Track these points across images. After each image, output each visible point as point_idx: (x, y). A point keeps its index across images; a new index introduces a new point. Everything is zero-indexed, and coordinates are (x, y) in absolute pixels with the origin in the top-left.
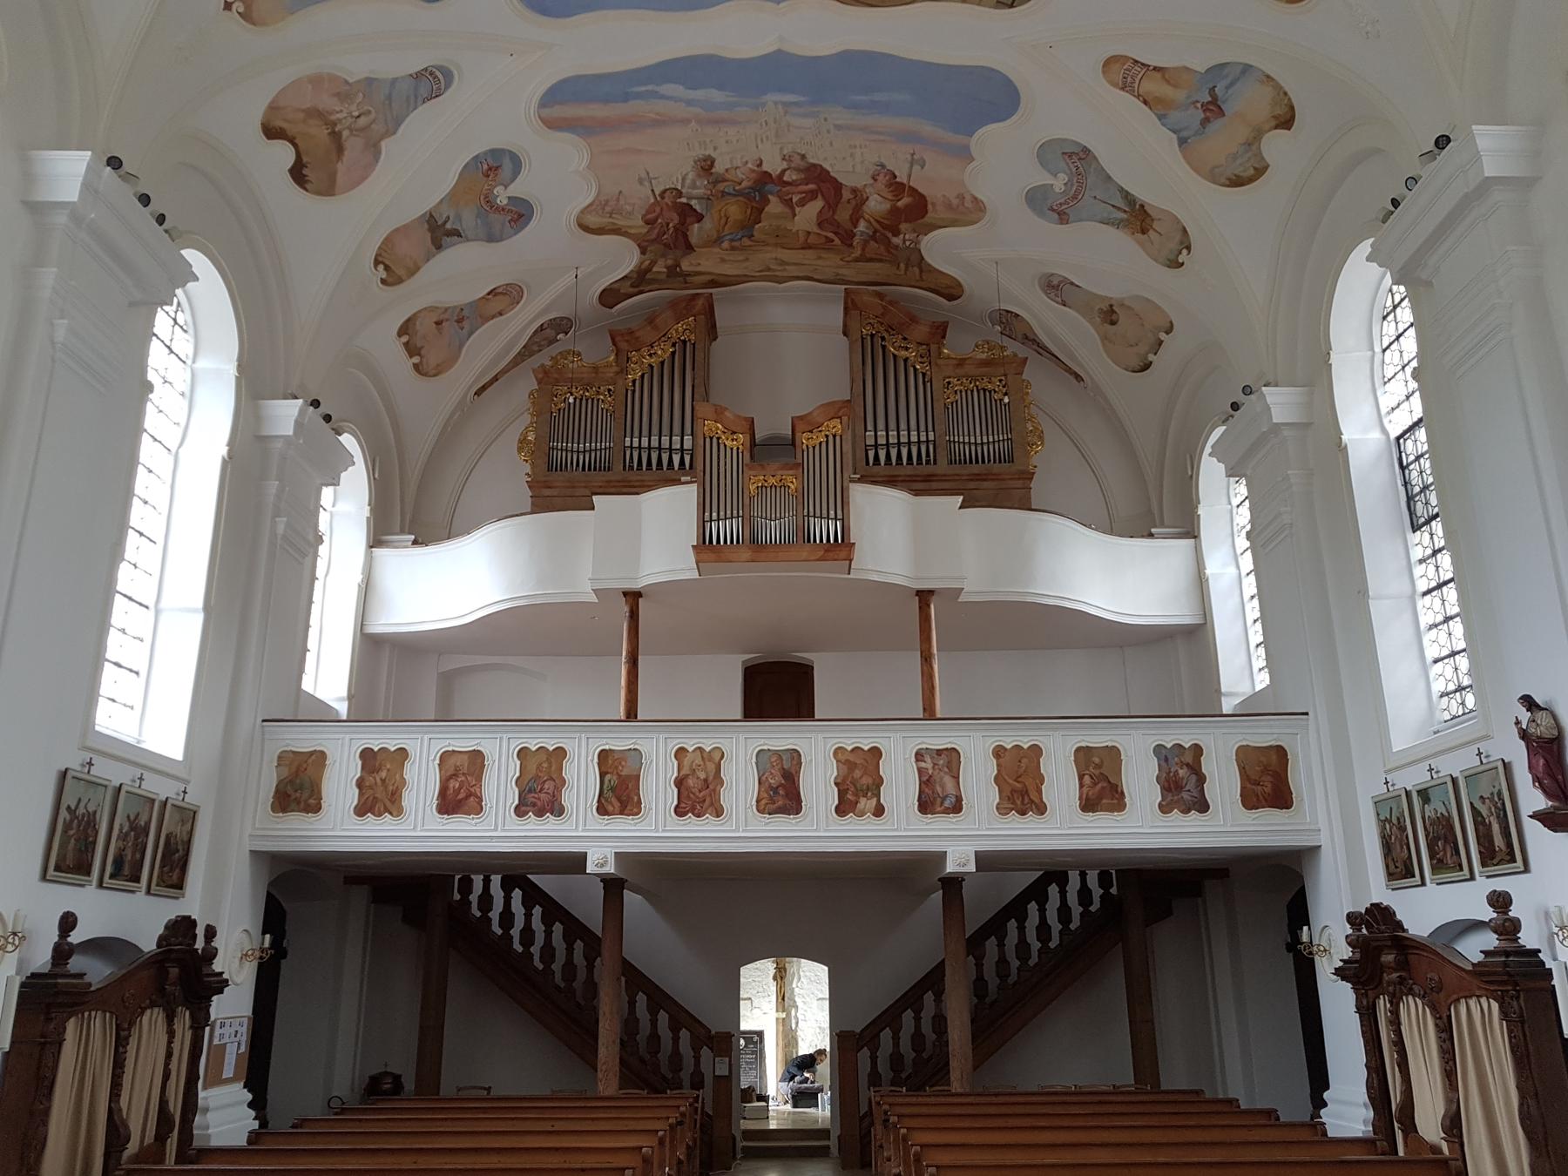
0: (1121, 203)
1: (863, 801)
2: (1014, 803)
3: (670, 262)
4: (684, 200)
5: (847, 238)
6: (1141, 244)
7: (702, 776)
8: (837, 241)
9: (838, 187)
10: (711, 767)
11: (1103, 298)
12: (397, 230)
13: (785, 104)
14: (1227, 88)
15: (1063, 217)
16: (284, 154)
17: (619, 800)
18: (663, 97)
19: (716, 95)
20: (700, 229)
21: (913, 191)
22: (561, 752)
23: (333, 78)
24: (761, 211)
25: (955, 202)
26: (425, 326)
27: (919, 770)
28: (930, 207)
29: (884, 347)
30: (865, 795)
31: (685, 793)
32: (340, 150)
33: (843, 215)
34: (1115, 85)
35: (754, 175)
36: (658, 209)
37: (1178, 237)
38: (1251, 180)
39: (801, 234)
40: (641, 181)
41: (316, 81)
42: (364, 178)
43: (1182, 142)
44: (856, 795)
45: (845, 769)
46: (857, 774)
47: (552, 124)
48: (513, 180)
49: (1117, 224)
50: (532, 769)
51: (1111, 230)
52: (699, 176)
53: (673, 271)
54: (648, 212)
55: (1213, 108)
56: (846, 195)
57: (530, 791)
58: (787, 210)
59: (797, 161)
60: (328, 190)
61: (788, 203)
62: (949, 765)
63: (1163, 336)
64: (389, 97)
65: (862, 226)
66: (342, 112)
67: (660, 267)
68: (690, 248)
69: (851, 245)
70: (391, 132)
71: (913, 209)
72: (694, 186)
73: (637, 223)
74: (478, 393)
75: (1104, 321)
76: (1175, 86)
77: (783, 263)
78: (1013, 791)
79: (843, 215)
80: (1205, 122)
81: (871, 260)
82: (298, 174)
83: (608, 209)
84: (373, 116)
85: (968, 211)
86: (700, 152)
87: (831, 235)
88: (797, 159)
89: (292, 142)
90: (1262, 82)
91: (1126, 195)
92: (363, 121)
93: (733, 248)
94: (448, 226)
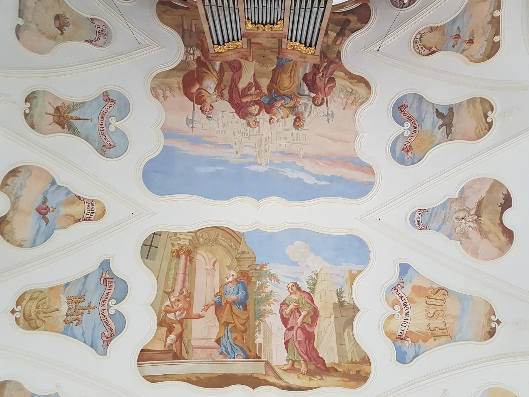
0: (77, 124)
4: (312, 95)
6: (57, 98)
9: (231, 100)
12: (471, 139)
13: (255, 163)
14: (40, 227)
16: (510, 218)
18: (314, 175)
19: (289, 173)
20: (305, 69)
23: (466, 249)
24: (273, 81)
25: (168, 93)
26: (480, 47)
28: (181, 86)
32: (479, 204)
33: (228, 75)
34: (98, 202)
35: (274, 111)
36: (326, 90)
37: (36, 120)
38: (7, 177)
39: (251, 58)
41: (475, 253)
42: (474, 181)
43: (53, 183)
47: (369, 170)
48: (397, 138)
54: (332, 88)
55: (43, 211)
56: (226, 93)
58: (258, 80)
59: (251, 120)
60: (496, 185)
61: (258, 87)
63: (21, 22)
64: (444, 222)
65: (217, 67)
66: (469, 226)
70: (451, 201)
71: (190, 80)
72: (306, 105)
73: (341, 82)
76: (67, 215)
80: (45, 201)
82: (507, 203)
83: (353, 97)
84: (456, 215)
85: (159, 87)
86: (300, 132)
88: (252, 124)
89: (501, 223)
90: (23, 240)
91: (74, 132)
92: (462, 215)
94: (441, 122)
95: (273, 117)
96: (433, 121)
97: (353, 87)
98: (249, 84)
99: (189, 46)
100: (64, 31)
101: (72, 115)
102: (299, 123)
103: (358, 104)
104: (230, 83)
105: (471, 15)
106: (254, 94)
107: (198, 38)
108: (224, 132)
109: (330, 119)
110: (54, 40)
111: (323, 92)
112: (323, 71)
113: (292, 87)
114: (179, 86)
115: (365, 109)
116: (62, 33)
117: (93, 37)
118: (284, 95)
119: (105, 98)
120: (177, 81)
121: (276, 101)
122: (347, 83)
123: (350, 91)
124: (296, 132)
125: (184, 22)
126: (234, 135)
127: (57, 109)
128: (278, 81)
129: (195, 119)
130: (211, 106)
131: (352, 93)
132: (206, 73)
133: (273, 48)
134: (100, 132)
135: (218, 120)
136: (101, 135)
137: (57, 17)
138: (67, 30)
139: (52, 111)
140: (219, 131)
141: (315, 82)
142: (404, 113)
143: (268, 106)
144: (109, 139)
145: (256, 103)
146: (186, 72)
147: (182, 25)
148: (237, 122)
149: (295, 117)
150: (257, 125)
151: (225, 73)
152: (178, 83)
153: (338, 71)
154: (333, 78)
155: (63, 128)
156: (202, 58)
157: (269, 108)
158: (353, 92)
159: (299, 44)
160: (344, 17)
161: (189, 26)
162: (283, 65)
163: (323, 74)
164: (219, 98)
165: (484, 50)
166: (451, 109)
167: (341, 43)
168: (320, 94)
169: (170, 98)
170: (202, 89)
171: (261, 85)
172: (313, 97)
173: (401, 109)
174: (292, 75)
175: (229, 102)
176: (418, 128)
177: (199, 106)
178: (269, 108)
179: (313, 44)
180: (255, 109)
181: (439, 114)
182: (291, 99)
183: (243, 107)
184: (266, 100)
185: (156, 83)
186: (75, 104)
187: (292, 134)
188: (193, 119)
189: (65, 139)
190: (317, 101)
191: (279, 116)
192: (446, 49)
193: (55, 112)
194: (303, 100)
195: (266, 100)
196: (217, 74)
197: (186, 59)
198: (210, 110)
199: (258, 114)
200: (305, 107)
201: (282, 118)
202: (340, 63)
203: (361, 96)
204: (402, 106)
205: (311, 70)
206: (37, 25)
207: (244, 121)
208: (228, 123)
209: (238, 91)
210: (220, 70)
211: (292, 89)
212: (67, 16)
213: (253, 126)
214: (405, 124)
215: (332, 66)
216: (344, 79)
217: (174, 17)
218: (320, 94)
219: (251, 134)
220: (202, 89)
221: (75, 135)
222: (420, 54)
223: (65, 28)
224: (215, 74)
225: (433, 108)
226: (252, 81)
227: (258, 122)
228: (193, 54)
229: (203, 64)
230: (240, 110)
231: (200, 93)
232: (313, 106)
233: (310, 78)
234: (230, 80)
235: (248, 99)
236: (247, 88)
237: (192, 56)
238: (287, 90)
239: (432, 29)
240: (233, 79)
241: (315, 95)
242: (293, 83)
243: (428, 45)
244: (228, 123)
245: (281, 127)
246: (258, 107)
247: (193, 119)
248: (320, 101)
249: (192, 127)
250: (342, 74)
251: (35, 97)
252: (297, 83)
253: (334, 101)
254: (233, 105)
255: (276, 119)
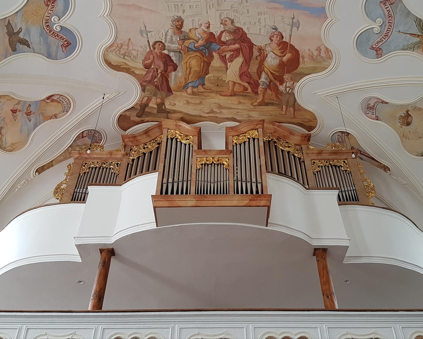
0: (415, 30)
3: (159, 101)
4: (166, 52)
5: (255, 85)
8: (250, 90)
9: (251, 45)
11: (401, 106)
15: (378, 52)
20: (175, 76)
21: (292, 47)
24: (209, 64)
25: (315, 53)
28: (301, 59)
29: (276, 147)
33: (253, 69)
35: (205, 36)
36: (151, 57)
39: (231, 84)
40: (141, 32)
48: (64, 13)
49: (412, 47)
51: (409, 52)
52: (175, 33)
53: (161, 107)
54: (146, 59)
56: (256, 53)
58: (223, 65)
59: (229, 26)
61: (223, 58)
65: (263, 76)
67: (153, 104)
68: (169, 91)
69: (257, 93)
72: (172, 42)
73: (138, 65)
74: (40, 170)
75: (403, 124)
77: (220, 107)
79: (253, 69)
81: (267, 104)
83: (122, 51)
85: (323, 59)
86: (176, 14)
87: (246, 85)
88: (229, 22)
93: (193, 93)
94: (21, 35)
95: (206, 30)
96: (29, 35)
97: (124, 61)
98: (232, 61)
99: (290, 94)
100: (405, 112)
101: (417, 39)
103: (115, 45)
104: (252, 62)
105: (21, 131)
106: (227, 51)
107: (281, 100)
108: (260, 14)
109: (143, 29)
110: (416, 107)
111: (155, 55)
112: (158, 74)
113: (188, 59)
114: (303, 59)
115: (107, 40)
116: (407, 112)
117: (380, 106)
118: (196, 51)
119: (381, 52)
120: (305, 64)
121: (203, 46)
122: (131, 64)
123: (126, 57)
124: (180, 14)
125: (292, 113)
126: (248, 10)
128: (202, 64)
129: (290, 27)
130: (272, 40)
131: (124, 56)
132: (275, 71)
133: (210, 92)
134: (393, 19)
135: (265, 26)
136: (393, 15)
137: (408, 124)
138: (402, 113)
140: (264, 14)
141: (164, 64)
142: (63, 39)
143: (211, 40)
144: (385, 10)
145: (224, 43)
146: (295, 72)
147: (294, 110)
148: (244, 24)
149: (182, 30)
150: (223, 21)
151: (256, 71)
152: (304, 62)
153: (142, 75)
154: (146, 68)
156: (278, 84)
157: (211, 38)
158: (122, 56)
159: (182, 141)
160: (143, 119)
161: (288, 110)
162: (198, 79)
163: (157, 71)
164: (263, 48)
167: (143, 98)
168: (158, 53)
169: (313, 50)
170: (280, 57)
171: (219, 60)
172: (164, 49)
173: (67, 43)
174: (188, 70)
175: (253, 44)
176: (44, 26)
177: (284, 40)
178: (211, 38)
179: (169, 141)
180: (225, 37)
181: (25, 43)
182: (188, 47)
183: (238, 39)
184: (215, 46)
185: (325, 63)
186: (412, 50)
187: (184, 12)
188: (292, 27)
190: (160, 46)
191: (200, 30)
192: (36, 102)
194: (175, 46)
195: (215, 46)
196: (264, 70)
197: (293, 83)
198: (273, 36)
199: (222, 32)
201: (197, 28)
202: (141, 81)
203: (114, 53)
204: (67, 46)
205: (170, 74)
208: (255, 23)
209: (243, 54)
210: (261, 73)
211: (188, 57)
212: (399, 124)
213: (228, 20)
214: (59, 29)
215: (149, 78)
216: (135, 68)
217: (302, 117)
218: (158, 53)
219: (230, 11)
220: (280, 57)
221: (420, 19)
222: (61, 95)
223: (404, 115)
224: (266, 70)
225: (33, 48)
226: (229, 64)
227: (222, 23)
228: (286, 87)
229: (278, 78)
230: (241, 36)
231: (282, 53)
233: (170, 68)
234: (251, 65)
236: (234, 57)
237: (288, 85)
238: (193, 55)
239: (56, 116)
240: (249, 66)
241: (163, 52)
242: (187, 62)
243: (55, 104)
244: (255, 23)
245: (196, 19)
246: (222, 39)
247: (292, 27)
248: (157, 46)
249: (293, 18)
250: (137, 72)
252: (183, 63)
253: (142, 47)
254: (249, 41)
255: (203, 27)
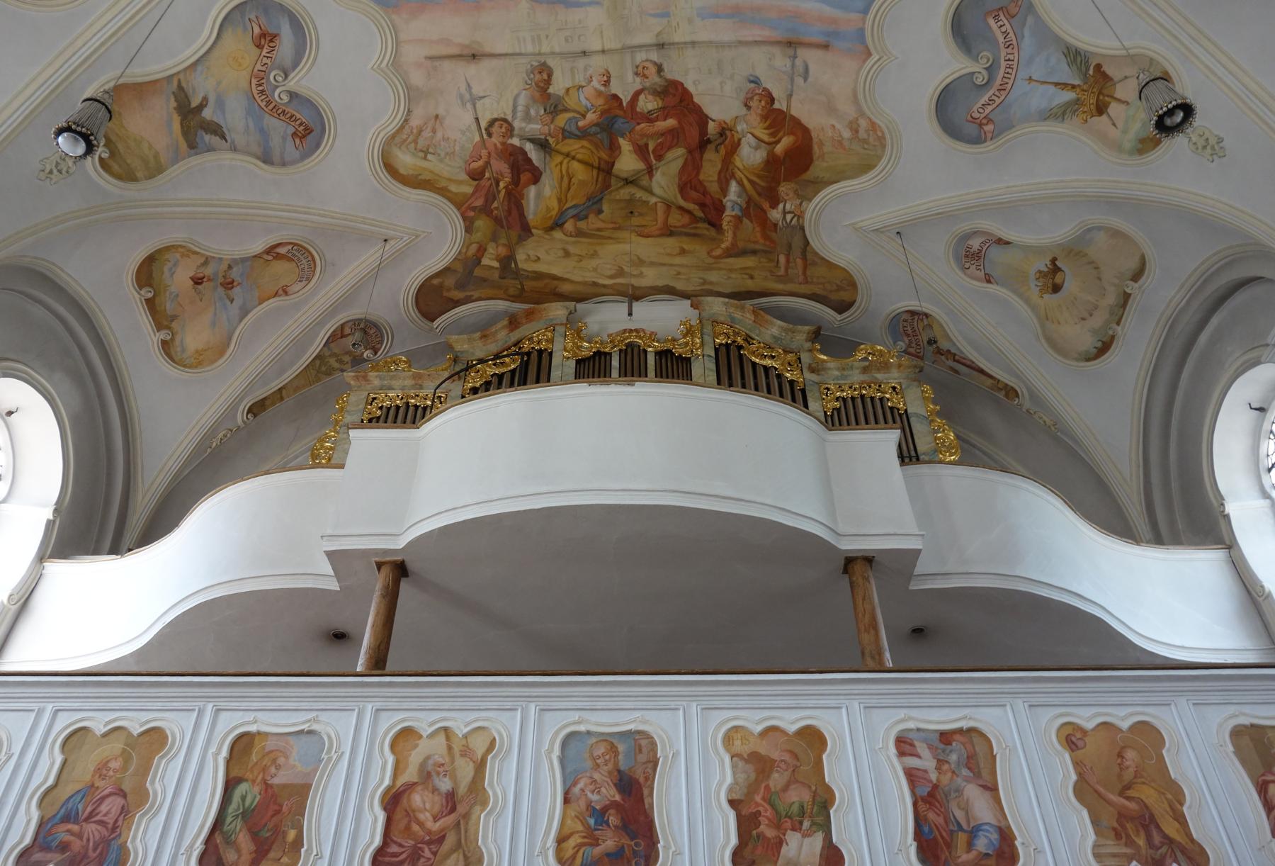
0: (1066, 74)
1: (793, 839)
2: (1130, 843)
4: (515, 141)
5: (711, 212)
7: (445, 785)
9: (703, 119)
10: (465, 771)
11: (1038, 251)
17: (254, 836)
20: (539, 195)
22: (155, 739)
26: (179, 277)
27: (911, 775)
28: (816, 148)
30: (796, 828)
31: (400, 823)
35: (600, 101)
36: (484, 153)
44: (778, 826)
45: (750, 771)
46: (777, 780)
50: (84, 772)
57: (66, 819)
59: (654, 79)
61: (641, 151)
62: (970, 760)
65: (733, 187)
74: (257, 409)
78: (1122, 816)
81: (743, 253)
88: (653, 70)
91: (1075, 56)
93: (580, 233)
94: (207, 114)
95: (602, 88)
99: (794, 227)
101: (1069, 96)
102: (538, 77)
107: (773, 242)
112: (499, 192)
116: (1054, 261)
117: (995, 253)
118: (579, 138)
121: (597, 125)
127: (1101, 110)
134: (1015, 51)
136: (1014, 42)
137: (1056, 289)
138: (1043, 264)
139: (1114, 109)
142: (296, 120)
145: (648, 118)
150: (640, 69)
154: (474, 179)
155: (1098, 67)
156: (766, 205)
163: (498, 185)
165: (166, 269)
166: (193, 146)
171: (634, 156)
172: (512, 136)
173: (305, 130)
174: (566, 180)
175: (707, 117)
177: (777, 106)
180: (647, 104)
181: (216, 130)
189: (1097, 40)
193: (1106, 105)
198: (752, 98)
200: (527, 113)
204: (304, 136)
205: (525, 191)
206: (1100, 279)
207: (669, 76)
224: (739, 174)
227: (637, 74)
228: (785, 213)
231: (772, 135)
232: (509, 118)
233: (525, 177)
235: (663, 125)
241: (510, 141)
248: (495, 129)
251: (1142, 141)
255: (595, 83)
